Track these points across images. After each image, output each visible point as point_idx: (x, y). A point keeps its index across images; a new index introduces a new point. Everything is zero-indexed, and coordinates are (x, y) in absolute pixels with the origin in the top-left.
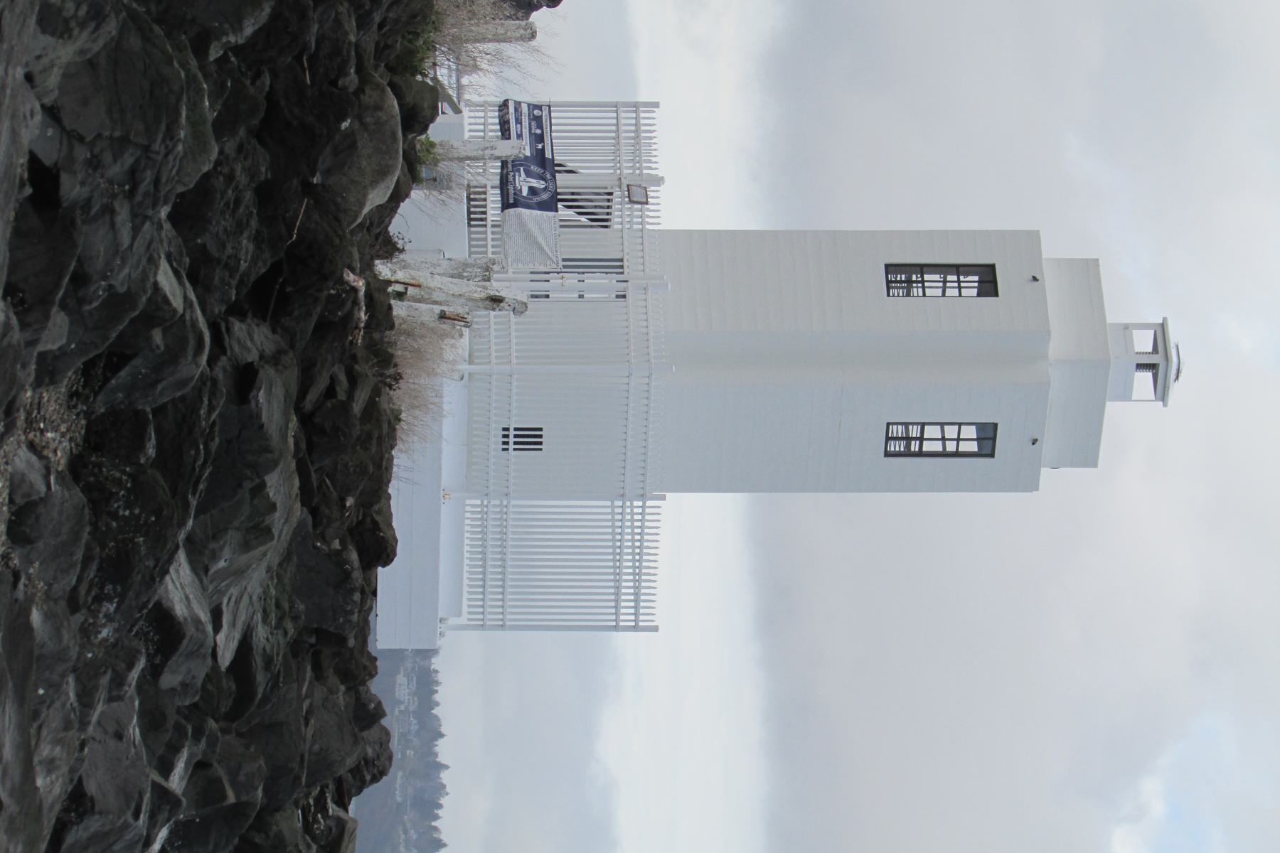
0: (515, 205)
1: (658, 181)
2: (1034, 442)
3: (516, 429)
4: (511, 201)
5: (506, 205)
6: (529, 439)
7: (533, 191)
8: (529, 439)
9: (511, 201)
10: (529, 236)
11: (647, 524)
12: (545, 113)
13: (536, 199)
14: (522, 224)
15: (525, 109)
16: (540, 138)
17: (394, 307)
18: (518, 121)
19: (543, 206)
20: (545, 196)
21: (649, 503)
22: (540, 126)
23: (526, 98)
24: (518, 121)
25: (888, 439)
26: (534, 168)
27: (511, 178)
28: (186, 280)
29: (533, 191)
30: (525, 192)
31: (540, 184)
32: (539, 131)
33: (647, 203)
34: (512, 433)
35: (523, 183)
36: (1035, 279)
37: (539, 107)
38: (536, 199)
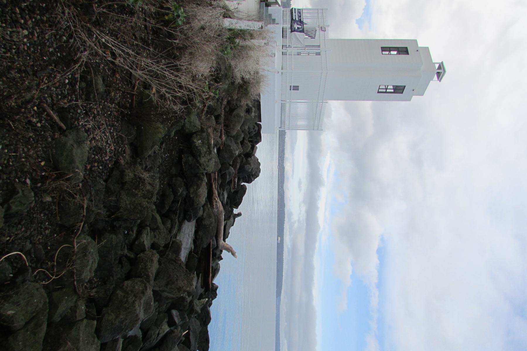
0: (294, 31)
1: (328, 26)
2: (413, 90)
3: (293, 86)
4: (293, 30)
5: (292, 31)
6: (296, 88)
7: (298, 28)
8: (296, 88)
9: (293, 30)
10: (298, 40)
11: (323, 104)
12: (301, 11)
13: (299, 30)
14: (295, 35)
15: (297, 10)
16: (300, 16)
17: (191, 223)
18: (295, 12)
19: (300, 32)
20: (301, 29)
21: (323, 104)
22: (300, 13)
23: (297, 8)
24: (295, 12)
25: (379, 89)
26: (299, 23)
27: (293, 25)
28: (200, 278)
29: (298, 28)
30: (296, 28)
31: (300, 27)
32: (300, 15)
33: (325, 31)
34: (292, 87)
35: (296, 26)
36: (417, 51)
37: (300, 10)
38: (299, 30)
